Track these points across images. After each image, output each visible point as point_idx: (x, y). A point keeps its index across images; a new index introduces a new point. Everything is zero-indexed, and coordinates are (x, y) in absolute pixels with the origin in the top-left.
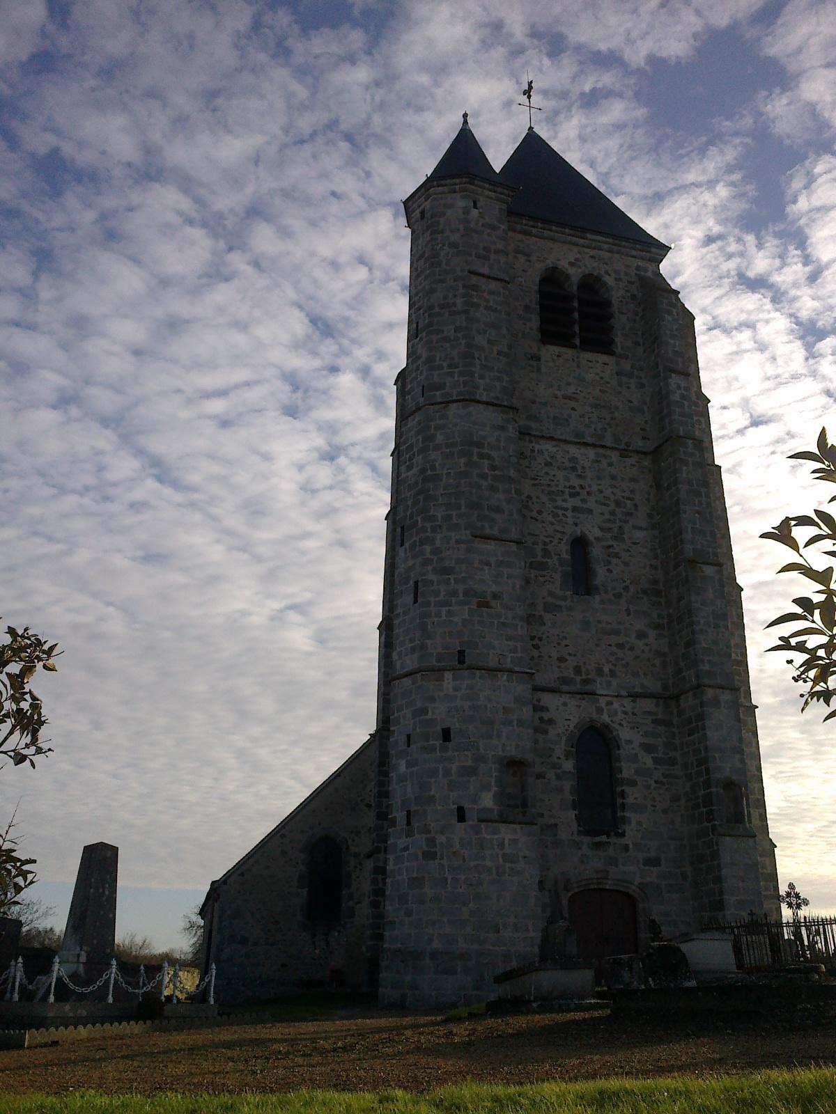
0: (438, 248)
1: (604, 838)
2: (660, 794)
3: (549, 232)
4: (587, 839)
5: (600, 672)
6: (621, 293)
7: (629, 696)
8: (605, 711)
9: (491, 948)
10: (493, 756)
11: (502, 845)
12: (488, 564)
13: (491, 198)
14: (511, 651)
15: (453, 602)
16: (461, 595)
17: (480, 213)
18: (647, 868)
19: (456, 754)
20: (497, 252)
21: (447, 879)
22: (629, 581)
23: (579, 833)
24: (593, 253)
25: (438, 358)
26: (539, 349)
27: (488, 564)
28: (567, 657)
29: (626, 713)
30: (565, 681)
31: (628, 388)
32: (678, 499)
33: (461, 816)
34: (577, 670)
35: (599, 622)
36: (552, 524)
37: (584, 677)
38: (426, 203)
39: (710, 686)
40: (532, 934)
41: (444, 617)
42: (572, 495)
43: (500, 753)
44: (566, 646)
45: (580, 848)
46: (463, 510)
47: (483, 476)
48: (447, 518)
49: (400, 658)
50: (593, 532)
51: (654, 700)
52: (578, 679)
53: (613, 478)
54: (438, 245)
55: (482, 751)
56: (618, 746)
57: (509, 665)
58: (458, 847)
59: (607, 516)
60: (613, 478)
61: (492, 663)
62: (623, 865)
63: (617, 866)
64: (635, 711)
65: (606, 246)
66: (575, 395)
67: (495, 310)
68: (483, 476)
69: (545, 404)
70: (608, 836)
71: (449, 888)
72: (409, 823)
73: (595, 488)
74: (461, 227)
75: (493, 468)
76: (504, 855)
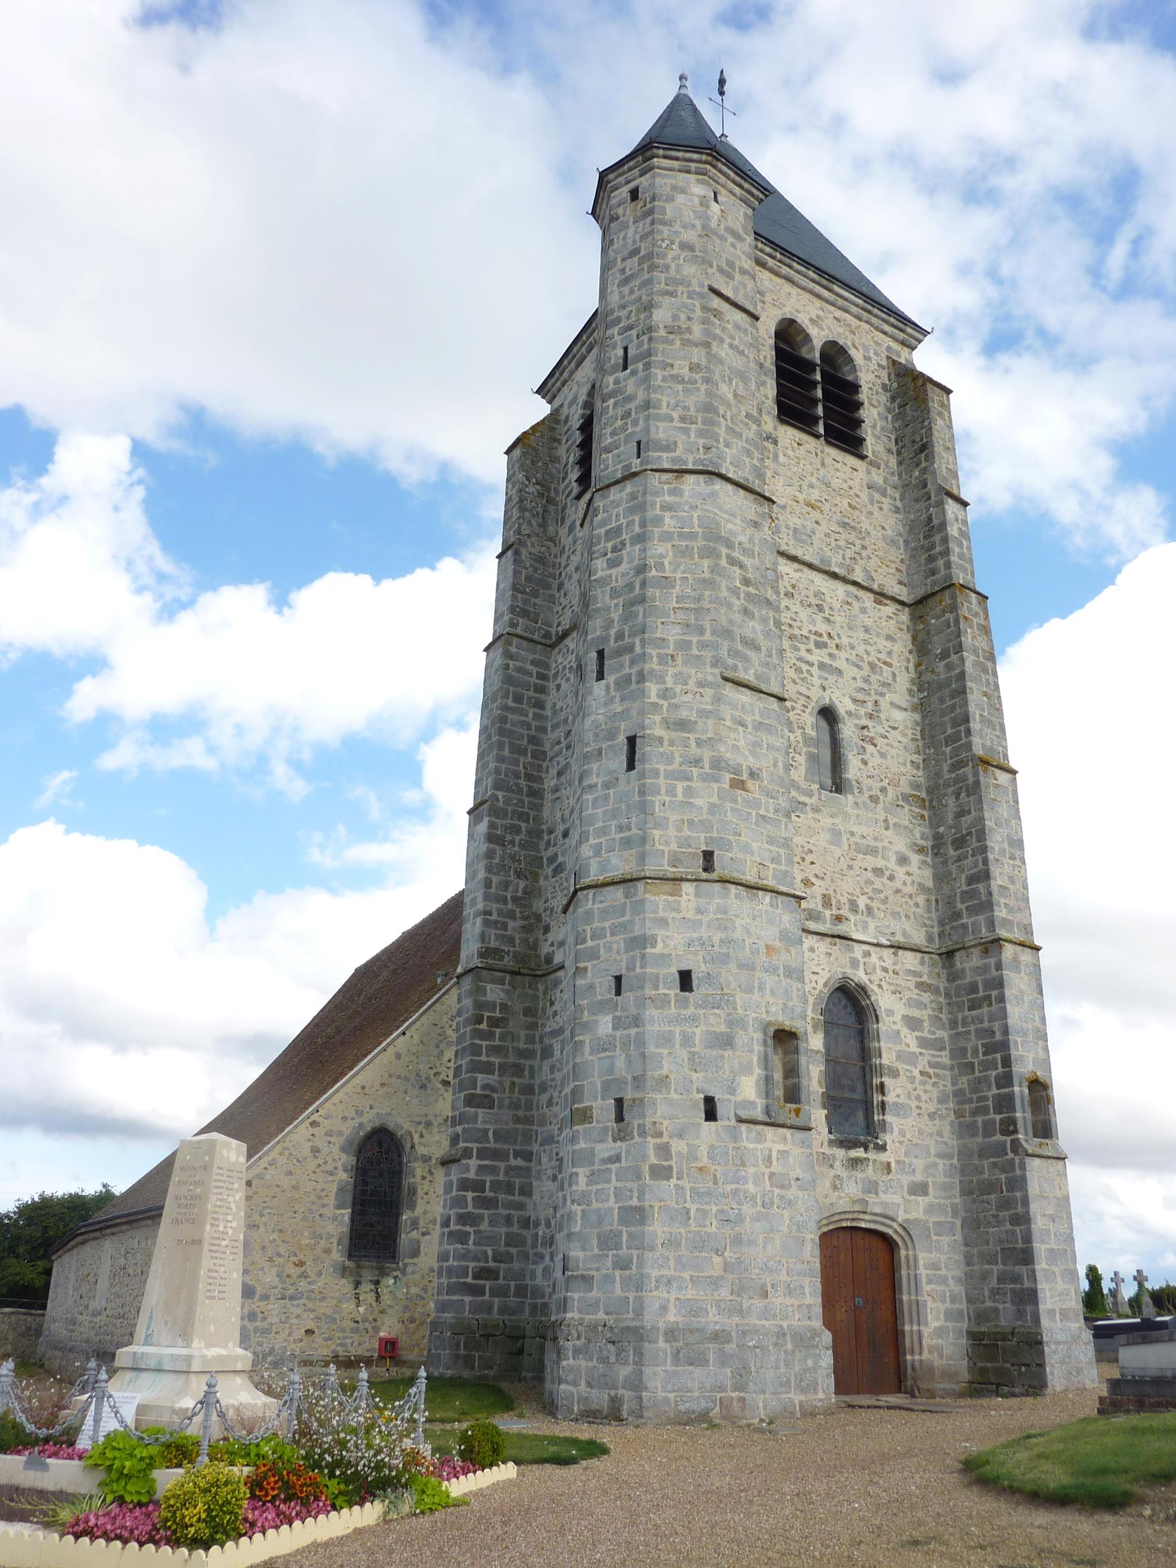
0: (664, 245)
1: (859, 1153)
2: (925, 1091)
4: (840, 1153)
5: (854, 907)
6: (871, 377)
7: (891, 946)
8: (862, 965)
9: (757, 1322)
11: (769, 1160)
12: (742, 724)
13: (734, 194)
15: (695, 775)
16: (707, 765)
18: (913, 1197)
19: (702, 1012)
21: (688, 1212)
22: (887, 781)
25: (665, 405)
27: (742, 724)
28: (813, 880)
29: (885, 970)
31: (881, 509)
32: (963, 673)
34: (827, 901)
35: (852, 834)
36: (794, 682)
37: (834, 912)
38: (642, 179)
39: (1010, 942)
40: (809, 1300)
41: (680, 797)
42: (819, 645)
43: (764, 1016)
44: (812, 863)
45: (831, 1166)
46: (707, 636)
48: (684, 645)
49: (598, 853)
50: (843, 706)
51: (919, 955)
52: (828, 913)
53: (867, 630)
54: (663, 240)
55: (740, 1011)
56: (877, 1017)
57: (770, 882)
58: (705, 1160)
61: (750, 877)
62: (885, 1192)
63: (877, 1194)
64: (897, 968)
65: (854, 309)
67: (742, 353)
68: (735, 591)
70: (866, 1149)
72: (620, 1118)
73: (845, 641)
74: (698, 223)
75: (746, 582)
76: (772, 1175)
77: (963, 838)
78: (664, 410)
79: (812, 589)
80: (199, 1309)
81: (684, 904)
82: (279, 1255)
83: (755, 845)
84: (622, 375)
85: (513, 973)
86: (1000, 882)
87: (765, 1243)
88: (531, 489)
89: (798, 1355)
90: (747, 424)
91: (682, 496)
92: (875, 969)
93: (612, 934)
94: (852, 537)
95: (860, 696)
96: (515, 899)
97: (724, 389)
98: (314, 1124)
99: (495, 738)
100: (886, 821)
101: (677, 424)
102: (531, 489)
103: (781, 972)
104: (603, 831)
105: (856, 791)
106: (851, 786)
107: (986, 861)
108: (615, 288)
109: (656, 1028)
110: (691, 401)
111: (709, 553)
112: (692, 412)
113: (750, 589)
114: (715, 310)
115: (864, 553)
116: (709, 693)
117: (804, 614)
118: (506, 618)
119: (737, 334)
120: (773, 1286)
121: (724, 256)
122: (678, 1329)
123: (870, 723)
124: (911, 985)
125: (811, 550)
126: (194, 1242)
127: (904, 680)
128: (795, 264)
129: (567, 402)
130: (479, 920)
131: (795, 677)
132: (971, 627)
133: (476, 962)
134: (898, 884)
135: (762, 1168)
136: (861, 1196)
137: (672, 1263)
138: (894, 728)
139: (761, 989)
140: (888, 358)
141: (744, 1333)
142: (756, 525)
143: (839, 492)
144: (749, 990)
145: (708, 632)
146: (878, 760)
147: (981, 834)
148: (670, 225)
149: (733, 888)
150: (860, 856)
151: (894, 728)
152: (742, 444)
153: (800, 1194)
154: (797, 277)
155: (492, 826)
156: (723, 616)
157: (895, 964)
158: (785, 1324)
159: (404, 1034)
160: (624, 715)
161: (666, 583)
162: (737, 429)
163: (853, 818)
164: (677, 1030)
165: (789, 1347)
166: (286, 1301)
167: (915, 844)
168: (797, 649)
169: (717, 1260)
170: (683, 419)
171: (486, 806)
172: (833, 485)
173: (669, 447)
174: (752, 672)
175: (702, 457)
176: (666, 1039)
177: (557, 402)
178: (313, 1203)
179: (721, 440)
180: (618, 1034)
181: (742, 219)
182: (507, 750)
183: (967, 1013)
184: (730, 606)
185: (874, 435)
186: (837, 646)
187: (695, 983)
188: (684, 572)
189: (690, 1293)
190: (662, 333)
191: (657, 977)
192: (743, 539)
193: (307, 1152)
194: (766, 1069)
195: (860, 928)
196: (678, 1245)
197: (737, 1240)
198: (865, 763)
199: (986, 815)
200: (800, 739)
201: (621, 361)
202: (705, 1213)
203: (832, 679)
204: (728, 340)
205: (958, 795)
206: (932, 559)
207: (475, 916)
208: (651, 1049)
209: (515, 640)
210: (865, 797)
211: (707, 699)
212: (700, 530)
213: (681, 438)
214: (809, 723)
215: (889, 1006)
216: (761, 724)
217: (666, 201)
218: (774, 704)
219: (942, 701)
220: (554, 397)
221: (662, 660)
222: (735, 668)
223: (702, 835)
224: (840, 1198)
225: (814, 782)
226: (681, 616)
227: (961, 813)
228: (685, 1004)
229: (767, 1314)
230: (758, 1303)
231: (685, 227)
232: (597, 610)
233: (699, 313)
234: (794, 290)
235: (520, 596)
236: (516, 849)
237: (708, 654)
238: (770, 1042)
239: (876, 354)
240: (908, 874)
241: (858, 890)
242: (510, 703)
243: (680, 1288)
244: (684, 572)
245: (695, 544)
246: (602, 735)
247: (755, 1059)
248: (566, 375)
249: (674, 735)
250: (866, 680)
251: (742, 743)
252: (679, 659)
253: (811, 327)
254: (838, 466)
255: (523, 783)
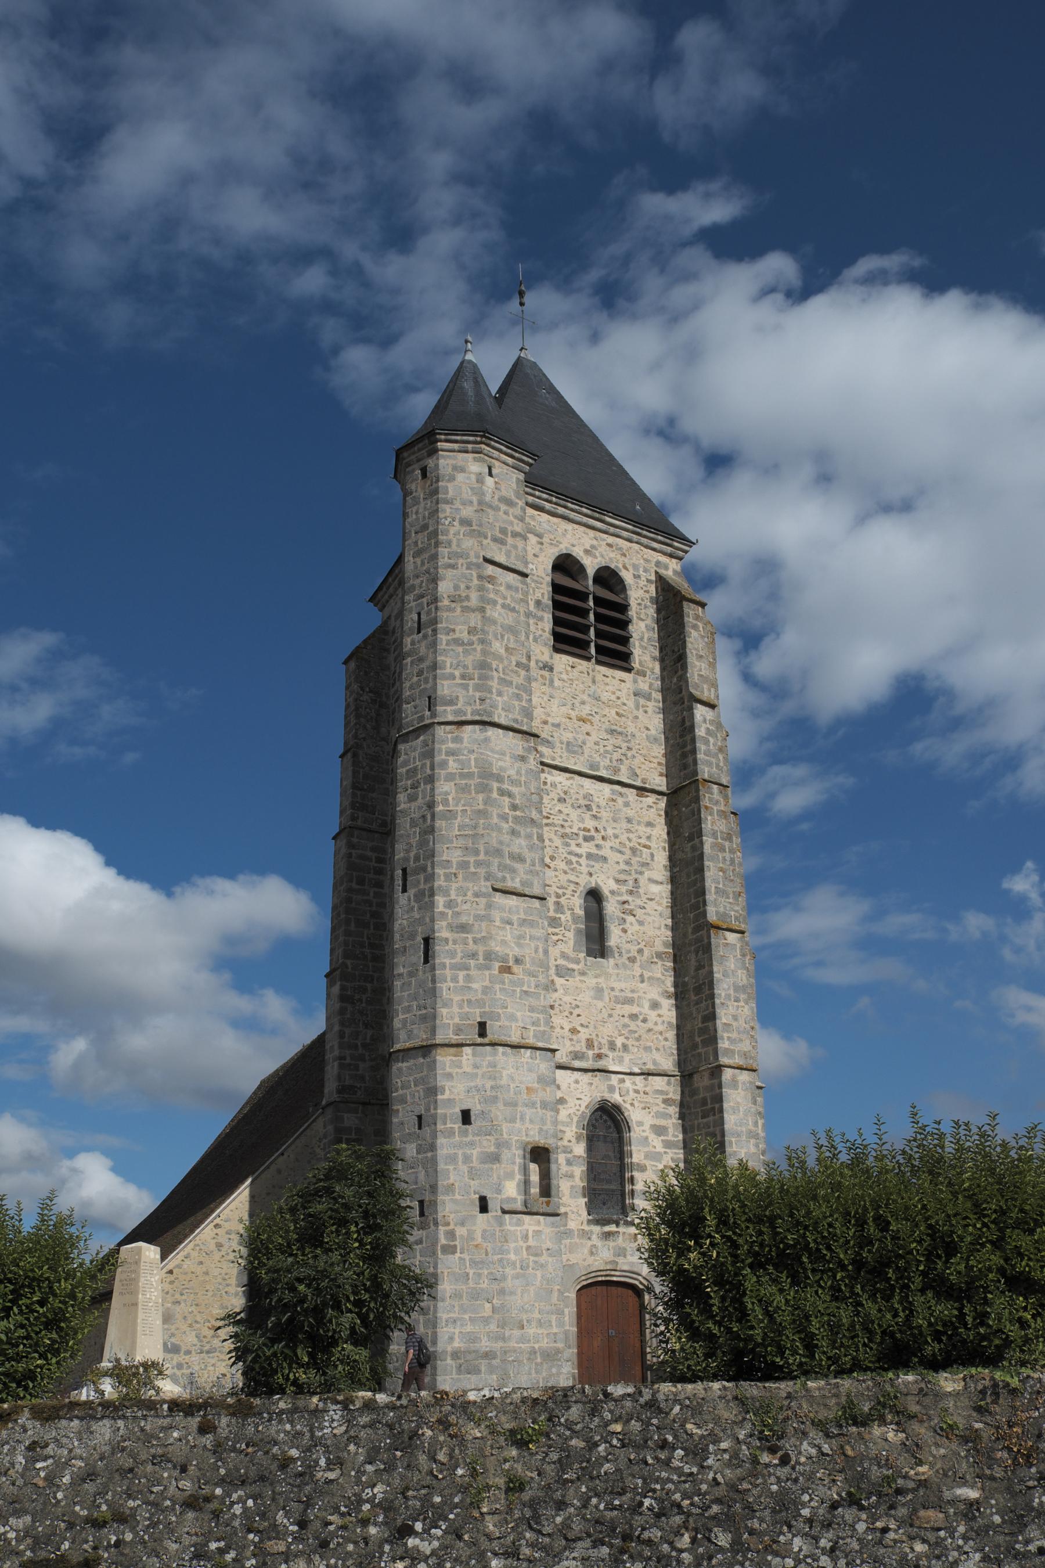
0: (447, 523)
1: (612, 1228)
3: (563, 510)
4: (597, 1229)
5: (612, 1046)
6: (641, 593)
8: (617, 1090)
10: (517, 1141)
11: (526, 1237)
12: (510, 923)
14: (533, 1024)
16: (481, 958)
17: (496, 483)
19: (477, 1138)
20: (515, 535)
21: (468, 1274)
23: (589, 1222)
24: (611, 539)
25: (448, 665)
26: (551, 657)
27: (510, 923)
28: (579, 1028)
29: (637, 1092)
30: (577, 1055)
31: (646, 712)
33: (484, 1206)
34: (590, 1044)
35: (613, 989)
36: (565, 872)
41: (461, 983)
42: (587, 839)
43: (524, 1138)
44: (579, 1015)
45: (589, 1238)
46: (482, 857)
47: (504, 817)
48: (464, 865)
50: (607, 886)
51: (666, 1078)
52: (590, 1053)
53: (629, 821)
54: (446, 518)
55: (505, 1136)
56: (629, 1127)
57: (531, 1041)
58: (480, 1240)
59: (623, 866)
60: (629, 821)
61: (515, 1039)
63: (625, 1256)
64: (647, 1089)
65: (625, 534)
66: (590, 717)
67: (513, 610)
68: (504, 817)
69: (558, 726)
70: (618, 1225)
71: (471, 1284)
73: (610, 832)
74: (475, 499)
75: (514, 807)
76: (528, 1248)
77: (700, 985)
78: (448, 670)
79: (581, 793)
80: (138, 1340)
81: (464, 1062)
82: (196, 1322)
83: (519, 1014)
84: (416, 637)
85: (364, 1104)
86: (724, 1021)
87: (522, 1293)
88: (365, 697)
89: (545, 1366)
90: (516, 672)
91: (462, 743)
92: (628, 1091)
93: (415, 1085)
94: (619, 741)
95: (622, 877)
96: (365, 1046)
97: (498, 647)
98: (217, 1226)
99: (343, 916)
100: (642, 976)
101: (458, 681)
102: (365, 697)
103: (538, 1106)
104: (408, 1009)
105: (617, 955)
106: (612, 951)
107: (713, 1004)
108: (411, 559)
109: (445, 1151)
110: (469, 661)
111: (484, 788)
112: (470, 670)
113: (518, 813)
114: (489, 576)
115: (629, 754)
116: (483, 901)
117: (574, 815)
118: (349, 812)
119: (508, 594)
120: (528, 1321)
121: (497, 525)
122: (460, 1352)
123: (630, 898)
124: (659, 1101)
125: (582, 759)
126: (133, 1304)
127: (662, 858)
128: (570, 505)
129: (394, 614)
130: (336, 1064)
131: (566, 868)
132: (711, 814)
133: (335, 1097)
134: (650, 1025)
135: (521, 1243)
136: (612, 1258)
137: (457, 1309)
138: (651, 900)
139: (522, 1119)
140: (657, 573)
141: (505, 1352)
142: (523, 759)
143: (607, 704)
144: (513, 1120)
145: (482, 853)
146: (636, 927)
147: (711, 984)
148: (452, 503)
149: (500, 1049)
150: (620, 1006)
151: (651, 900)
152: (512, 690)
153: (550, 1259)
154: (572, 515)
155: (343, 988)
156: (494, 839)
157: (646, 1086)
158: (536, 1346)
159: (282, 1154)
160: (420, 921)
161: (451, 815)
162: (508, 678)
163: (614, 977)
164: (460, 1152)
165: (539, 1360)
166: (204, 1355)
167: (666, 992)
168: (568, 845)
169: (488, 1306)
170: (463, 677)
171: (338, 972)
172: (603, 699)
173: (452, 702)
174: (518, 880)
175: (478, 707)
176: (452, 1159)
177: (387, 610)
178: (220, 1284)
179: (494, 691)
180: (420, 1156)
181: (514, 486)
182: (353, 924)
183: (700, 1120)
184: (499, 830)
185: (641, 646)
186: (603, 838)
187: (473, 1118)
188: (464, 805)
189: (469, 1328)
190: (446, 602)
191: (445, 1115)
192: (512, 772)
193: (212, 1246)
194: (525, 1175)
195: (617, 1062)
196: (461, 1297)
197: (502, 1292)
198: (625, 931)
199: (715, 969)
200: (569, 918)
201: (416, 625)
202: (480, 1275)
203: (597, 866)
204: (500, 601)
205: (697, 952)
206: (684, 755)
207: (334, 1061)
208: (441, 1166)
209: (356, 832)
210: (624, 959)
211: (482, 906)
212: (476, 770)
213: (461, 694)
214: (577, 904)
215: (639, 1119)
216: (524, 920)
217: (449, 481)
218: (536, 903)
219: (688, 876)
220: (384, 607)
221: (447, 877)
222: (504, 879)
223: (478, 1011)
224: (596, 1260)
225: (581, 952)
226: (461, 842)
227: (700, 967)
228: (465, 1133)
229: (523, 1339)
230: (517, 1333)
231: (464, 504)
232: (402, 836)
233: (476, 582)
234: (570, 526)
235: (359, 793)
236: (364, 1005)
237: (482, 871)
238: (528, 1156)
239: (645, 571)
240: (659, 1016)
241: (617, 1032)
242: (354, 885)
243: (462, 1325)
244: (464, 805)
245: (471, 782)
246: (406, 936)
247: (517, 1168)
248: (391, 590)
249: (456, 935)
250: (627, 863)
251: (509, 937)
252: (460, 876)
253: (585, 558)
254: (607, 680)
255: (367, 951)
